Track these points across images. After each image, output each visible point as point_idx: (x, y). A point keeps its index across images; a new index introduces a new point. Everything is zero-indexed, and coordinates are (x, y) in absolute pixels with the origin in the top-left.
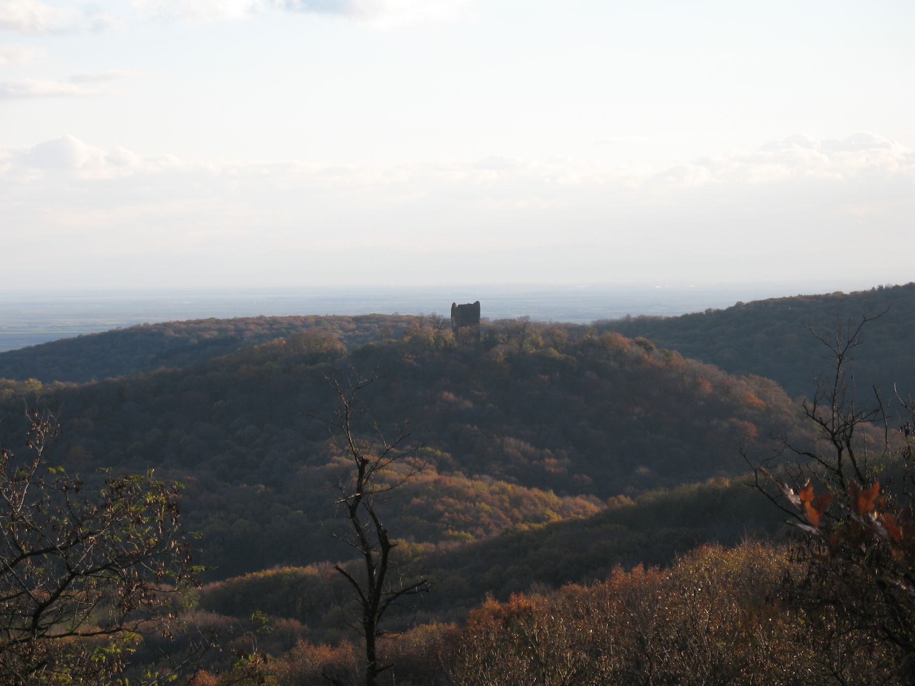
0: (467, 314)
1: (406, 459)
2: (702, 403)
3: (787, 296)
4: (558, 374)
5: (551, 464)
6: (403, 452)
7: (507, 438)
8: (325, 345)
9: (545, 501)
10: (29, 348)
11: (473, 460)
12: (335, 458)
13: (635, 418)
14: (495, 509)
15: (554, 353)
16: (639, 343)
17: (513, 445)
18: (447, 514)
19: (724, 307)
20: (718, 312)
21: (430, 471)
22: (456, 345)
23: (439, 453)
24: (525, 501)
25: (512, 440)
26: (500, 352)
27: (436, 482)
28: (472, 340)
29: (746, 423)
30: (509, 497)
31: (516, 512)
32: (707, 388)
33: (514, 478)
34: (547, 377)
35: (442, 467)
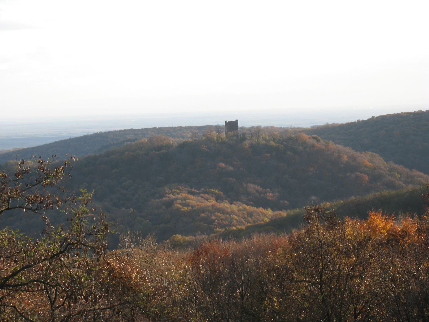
0: (232, 126)
1: (201, 195)
2: (343, 165)
3: (396, 113)
4: (274, 153)
5: (270, 195)
6: (200, 192)
7: (249, 184)
8: (165, 142)
9: (264, 214)
10: (46, 145)
11: (232, 194)
12: (167, 195)
13: (310, 173)
14: (240, 218)
15: (272, 143)
16: (314, 138)
17: (252, 187)
18: (216, 221)
19: (366, 119)
20: (363, 121)
21: (212, 200)
22: (227, 140)
23: (217, 191)
24: (255, 214)
25: (251, 185)
26: (247, 143)
27: (213, 206)
28: (235, 138)
29: (363, 174)
30: (247, 213)
31: (250, 219)
32: (345, 158)
33: (252, 203)
34: (269, 155)
35: (218, 198)
